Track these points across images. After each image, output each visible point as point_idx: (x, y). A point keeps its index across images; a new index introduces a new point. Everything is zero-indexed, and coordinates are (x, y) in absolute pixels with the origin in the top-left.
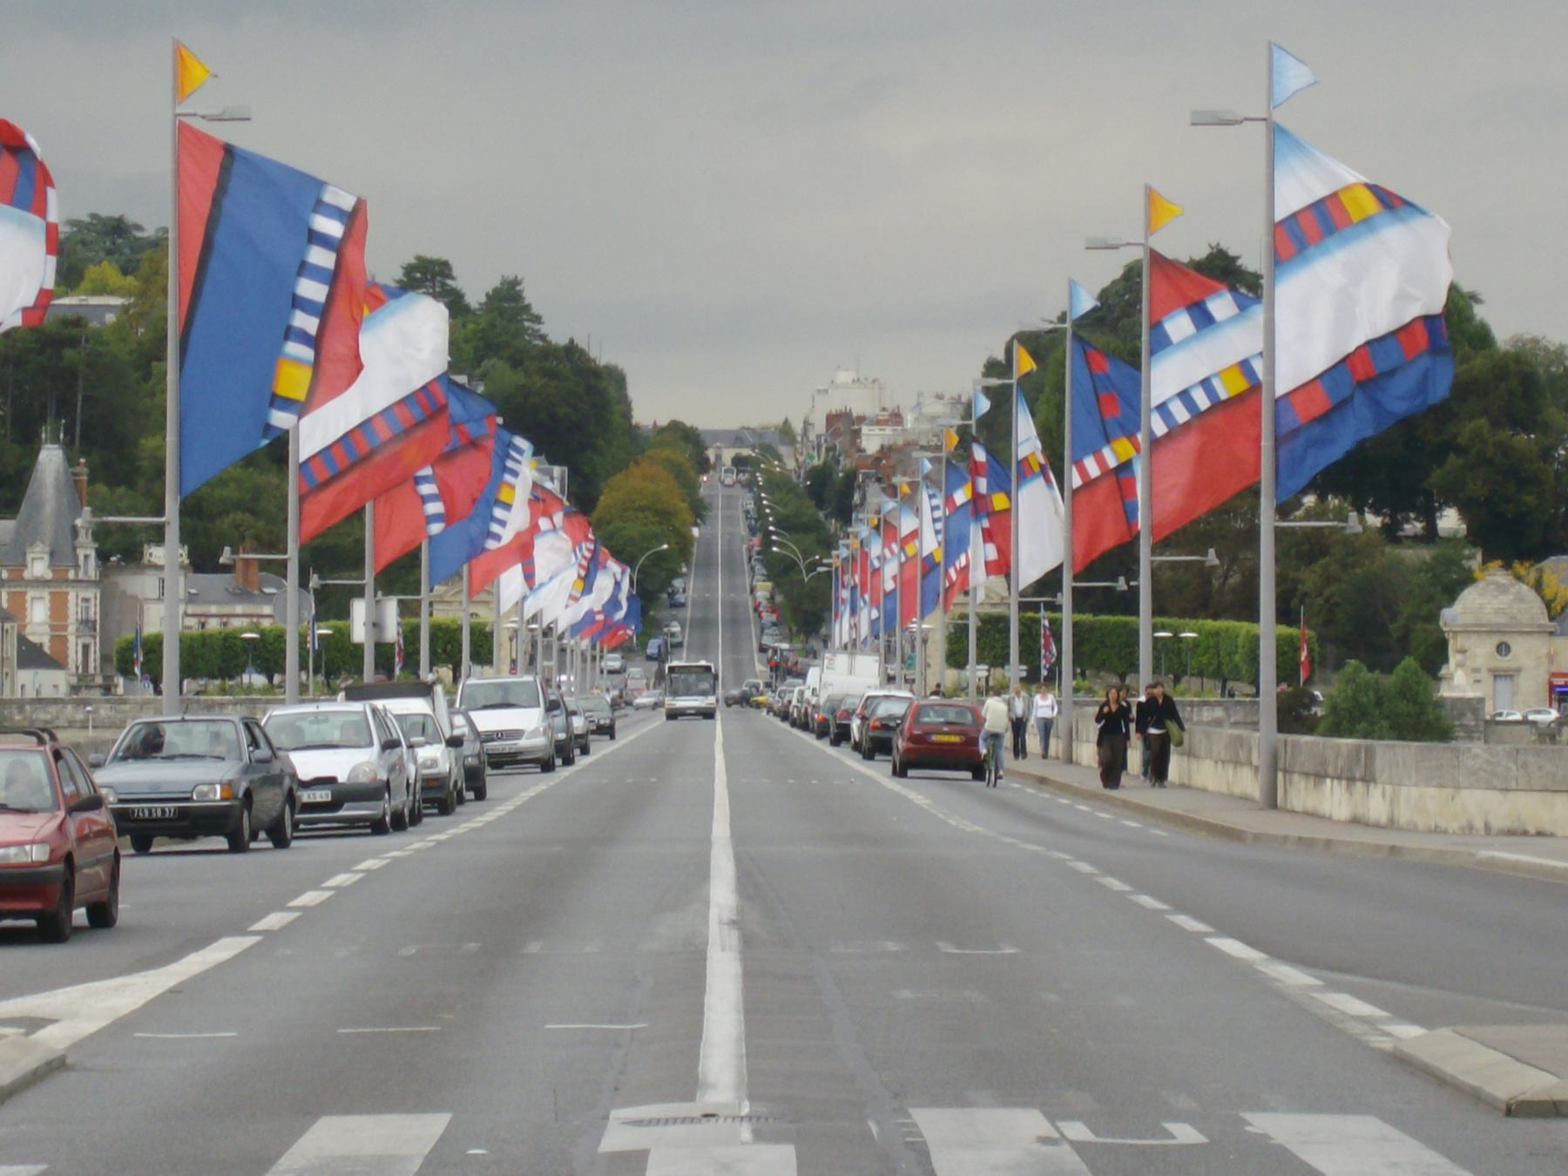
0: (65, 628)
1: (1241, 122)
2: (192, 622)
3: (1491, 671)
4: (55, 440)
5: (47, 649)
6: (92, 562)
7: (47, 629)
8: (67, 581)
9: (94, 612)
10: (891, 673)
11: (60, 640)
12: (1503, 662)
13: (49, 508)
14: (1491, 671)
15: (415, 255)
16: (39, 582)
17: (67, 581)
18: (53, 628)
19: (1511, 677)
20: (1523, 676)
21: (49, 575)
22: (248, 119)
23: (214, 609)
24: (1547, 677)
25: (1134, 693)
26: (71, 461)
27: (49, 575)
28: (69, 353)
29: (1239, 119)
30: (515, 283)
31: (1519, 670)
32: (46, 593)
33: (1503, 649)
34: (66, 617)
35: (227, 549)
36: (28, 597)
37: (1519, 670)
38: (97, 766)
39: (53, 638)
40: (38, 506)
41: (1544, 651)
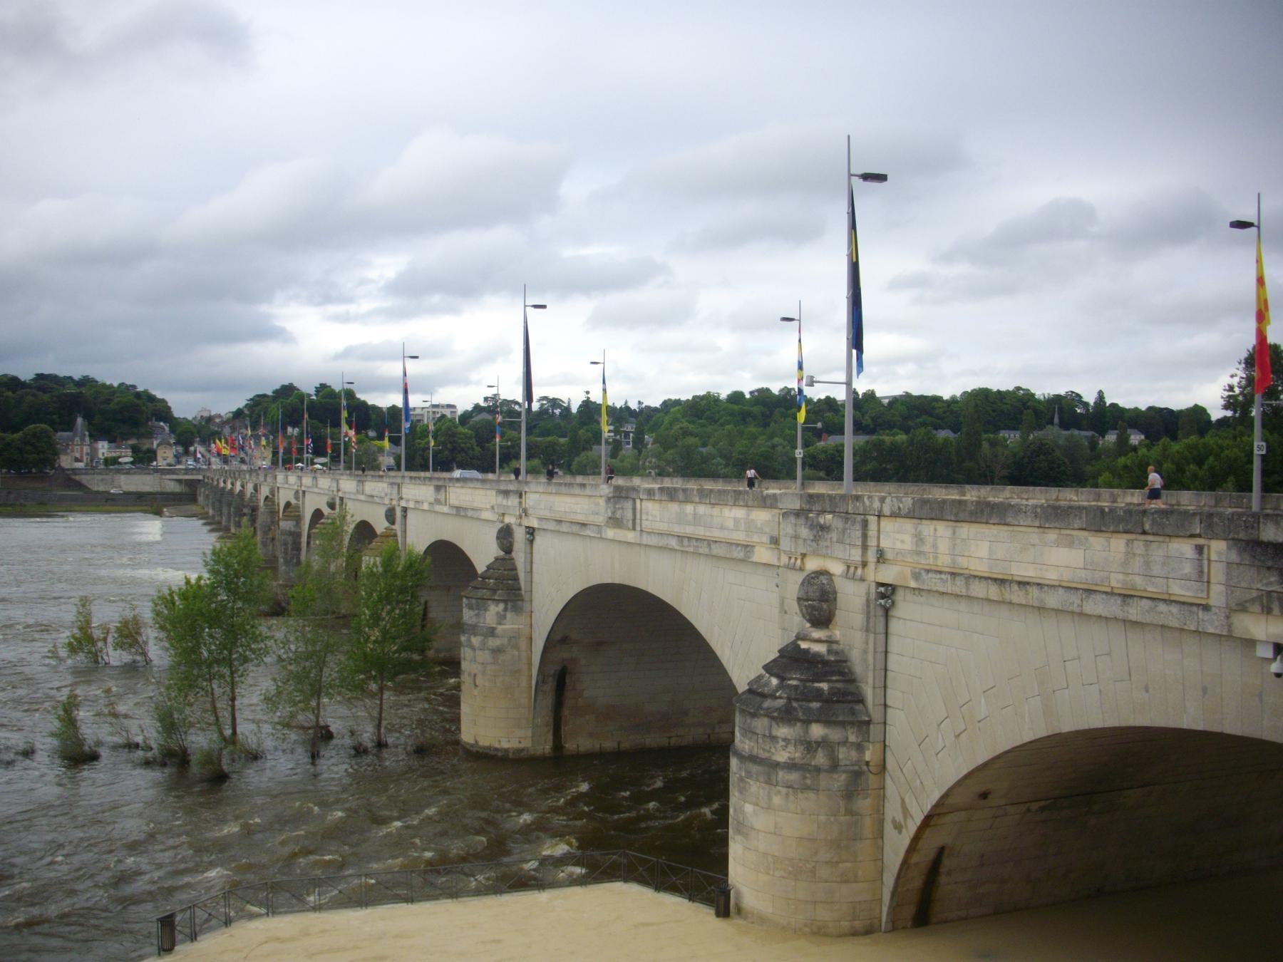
9: (89, 451)
11: (82, 457)
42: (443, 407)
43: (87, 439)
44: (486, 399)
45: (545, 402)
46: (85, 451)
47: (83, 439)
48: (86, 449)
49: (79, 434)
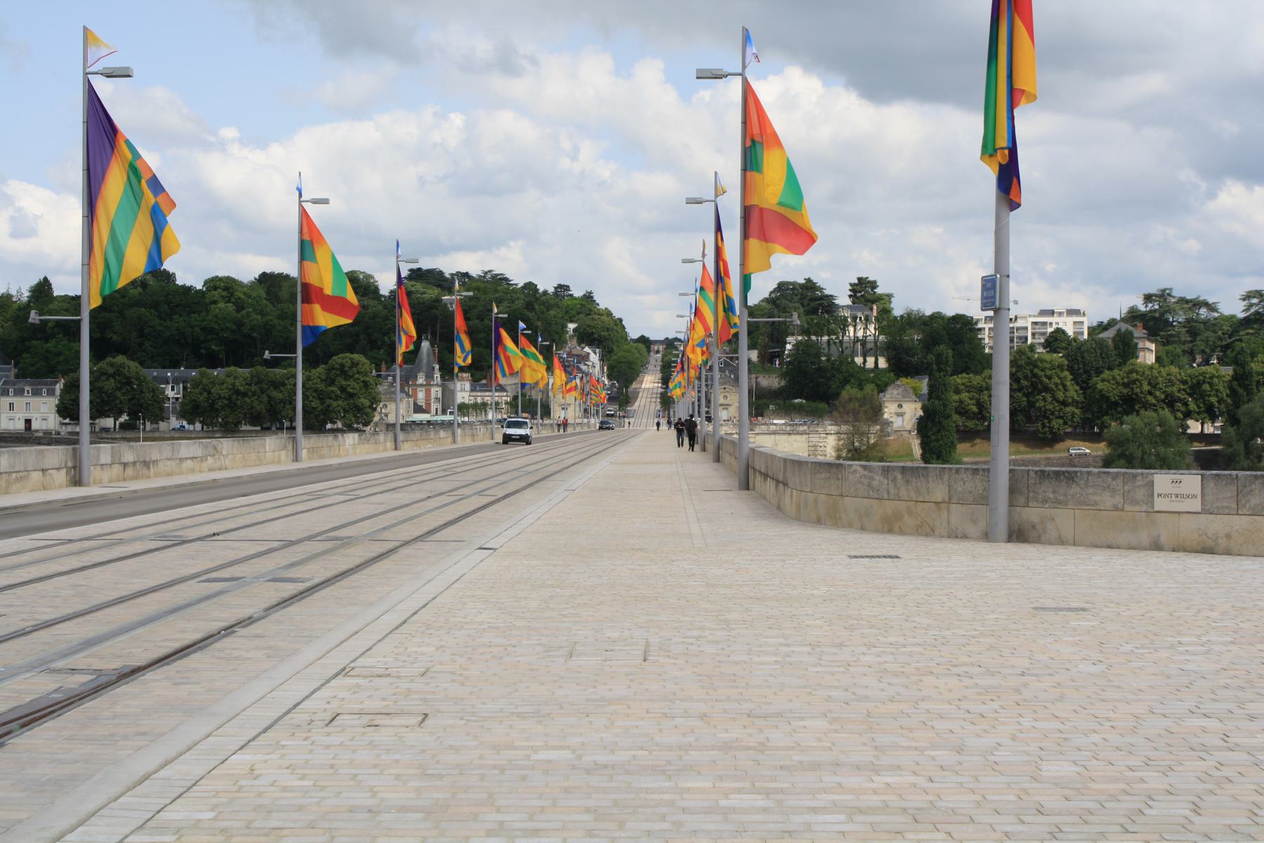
0: (430, 400)
1: (727, 76)
2: (472, 398)
3: (895, 413)
4: (427, 339)
5: (424, 407)
6: (439, 379)
7: (424, 401)
8: (431, 385)
9: (440, 395)
10: (900, 419)
11: (428, 405)
12: (900, 410)
13: (425, 361)
14: (895, 413)
15: (607, 307)
16: (422, 385)
17: (431, 385)
18: (426, 400)
19: (903, 415)
20: (906, 414)
21: (425, 383)
22: (129, 76)
23: (479, 394)
24: (1168, 287)
25: (307, 416)
26: (432, 345)
27: (425, 383)
28: (435, 311)
29: (725, 74)
30: (591, 293)
31: (905, 413)
32: (423, 389)
33: (900, 406)
34: (430, 397)
35: (267, 352)
36: (418, 390)
37: (905, 413)
38: (308, 452)
39: (426, 404)
40: (421, 361)
41: (914, 407)
42: (1060, 314)
43: (437, 375)
44: (1148, 298)
45: (1255, 301)
46: (433, 396)
47: (429, 376)
48: (436, 392)
49: (424, 368)
